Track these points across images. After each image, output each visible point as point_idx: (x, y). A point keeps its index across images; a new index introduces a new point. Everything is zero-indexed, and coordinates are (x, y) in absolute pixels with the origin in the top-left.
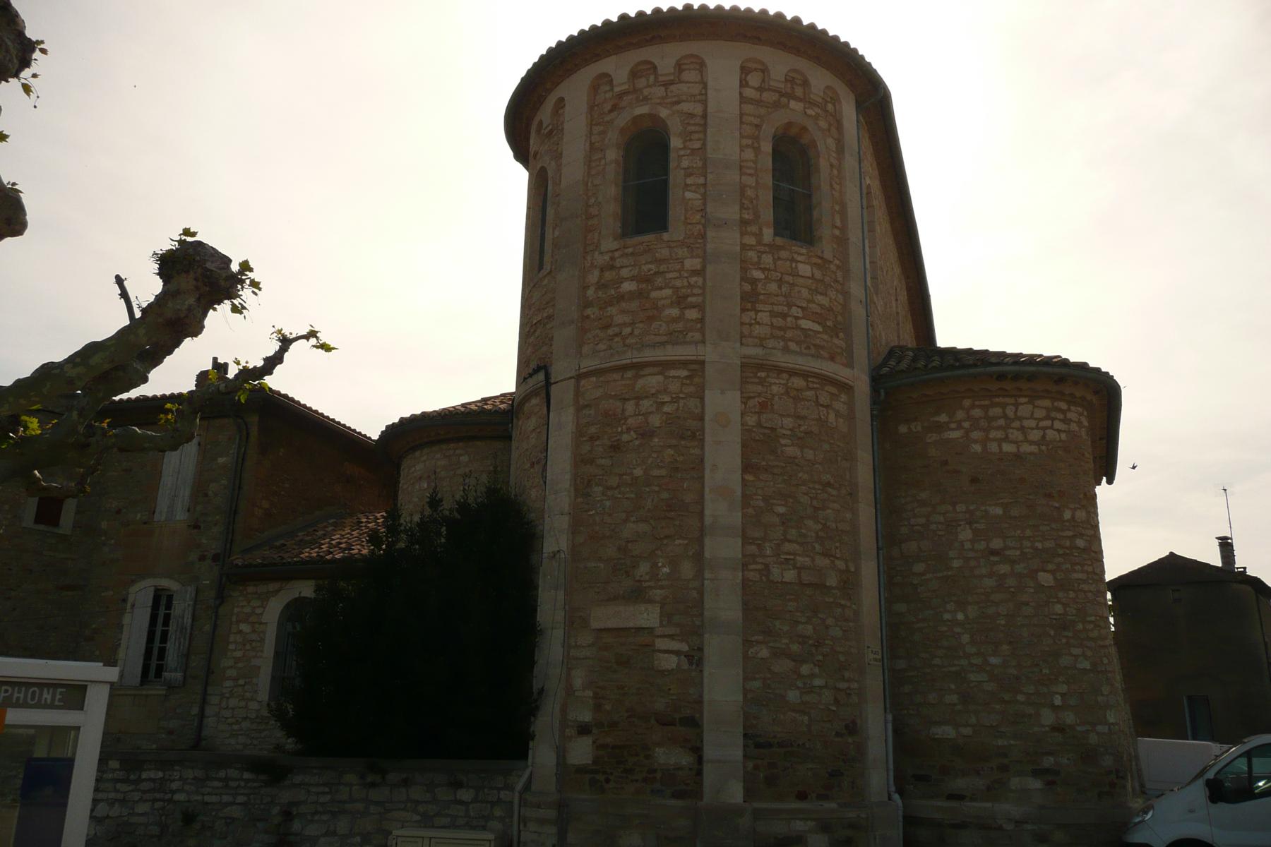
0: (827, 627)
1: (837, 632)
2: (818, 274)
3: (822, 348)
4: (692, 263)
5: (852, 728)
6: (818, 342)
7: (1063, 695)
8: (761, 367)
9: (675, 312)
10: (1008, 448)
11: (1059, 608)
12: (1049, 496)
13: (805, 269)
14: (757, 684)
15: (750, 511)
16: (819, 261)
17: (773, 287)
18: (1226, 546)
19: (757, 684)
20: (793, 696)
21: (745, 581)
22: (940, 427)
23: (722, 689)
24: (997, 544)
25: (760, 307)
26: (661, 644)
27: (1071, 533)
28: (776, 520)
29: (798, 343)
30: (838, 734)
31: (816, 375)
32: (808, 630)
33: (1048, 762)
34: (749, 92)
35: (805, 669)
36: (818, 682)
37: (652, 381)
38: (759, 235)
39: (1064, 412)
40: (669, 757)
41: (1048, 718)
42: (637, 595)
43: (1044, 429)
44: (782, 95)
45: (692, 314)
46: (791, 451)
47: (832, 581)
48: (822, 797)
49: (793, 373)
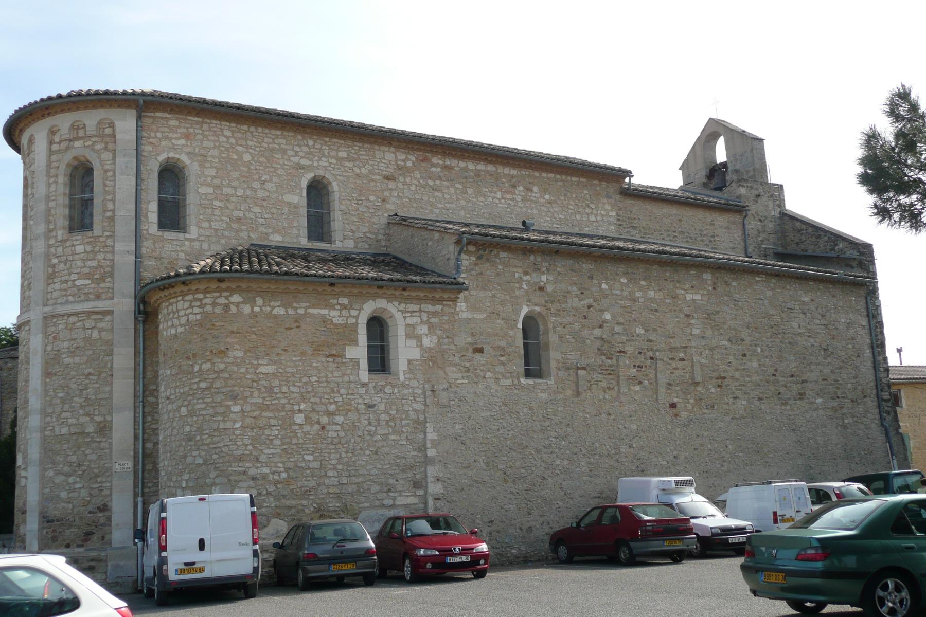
0: (86, 456)
1: (94, 457)
2: (89, 248)
3: (90, 293)
5: (104, 508)
6: (86, 291)
7: (187, 481)
8: (53, 316)
12: (188, 358)
13: (80, 249)
14: (48, 490)
15: (48, 398)
16: (91, 239)
17: (62, 266)
19: (48, 490)
20: (63, 495)
25: (56, 280)
27: (197, 380)
28: (58, 401)
29: (74, 296)
30: (90, 512)
31: (83, 312)
32: (74, 458)
35: (71, 480)
36: (77, 486)
39: (200, 300)
43: (188, 315)
44: (70, 140)
46: (67, 360)
47: (90, 429)
48: (79, 546)
49: (69, 315)
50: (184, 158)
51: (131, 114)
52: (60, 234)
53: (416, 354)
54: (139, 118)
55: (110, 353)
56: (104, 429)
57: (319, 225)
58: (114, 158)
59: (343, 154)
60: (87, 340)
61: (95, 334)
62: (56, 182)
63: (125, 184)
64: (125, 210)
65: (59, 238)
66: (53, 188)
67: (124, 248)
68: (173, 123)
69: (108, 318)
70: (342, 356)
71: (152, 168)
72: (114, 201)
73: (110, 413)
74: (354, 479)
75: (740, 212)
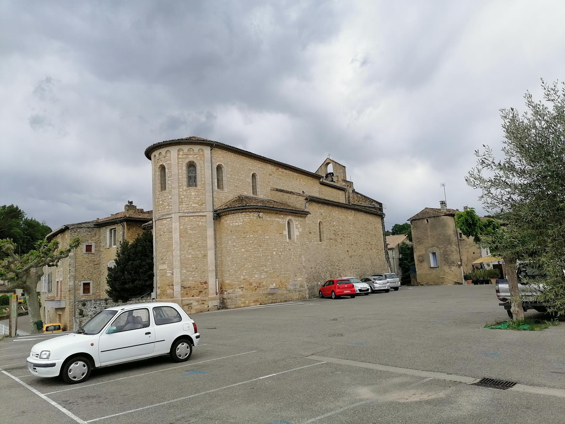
2: (197, 193)
4: (170, 197)
5: (206, 283)
9: (167, 207)
10: (237, 224)
11: (245, 256)
13: (193, 193)
17: (186, 199)
18: (443, 203)
20: (191, 278)
21: (181, 259)
22: (226, 220)
23: (177, 279)
24: (234, 244)
26: (168, 272)
33: (242, 286)
34: (180, 156)
35: (193, 273)
37: (165, 222)
38: (183, 188)
40: (169, 291)
41: (242, 277)
42: (164, 263)
45: (170, 207)
50: (223, 164)
51: (209, 148)
52: (185, 188)
53: (298, 234)
54: (211, 150)
55: (206, 230)
56: (205, 256)
57: (349, 203)
58: (204, 163)
59: (260, 166)
60: (198, 225)
61: (200, 223)
62: (182, 169)
63: (208, 172)
64: (209, 181)
65: (184, 189)
66: (180, 171)
67: (209, 194)
68: (220, 152)
69: (204, 218)
70: (282, 233)
71: (215, 167)
72: (204, 177)
73: (207, 250)
74: (288, 272)
75: (344, 190)
